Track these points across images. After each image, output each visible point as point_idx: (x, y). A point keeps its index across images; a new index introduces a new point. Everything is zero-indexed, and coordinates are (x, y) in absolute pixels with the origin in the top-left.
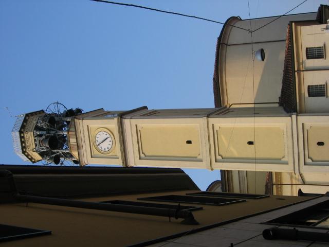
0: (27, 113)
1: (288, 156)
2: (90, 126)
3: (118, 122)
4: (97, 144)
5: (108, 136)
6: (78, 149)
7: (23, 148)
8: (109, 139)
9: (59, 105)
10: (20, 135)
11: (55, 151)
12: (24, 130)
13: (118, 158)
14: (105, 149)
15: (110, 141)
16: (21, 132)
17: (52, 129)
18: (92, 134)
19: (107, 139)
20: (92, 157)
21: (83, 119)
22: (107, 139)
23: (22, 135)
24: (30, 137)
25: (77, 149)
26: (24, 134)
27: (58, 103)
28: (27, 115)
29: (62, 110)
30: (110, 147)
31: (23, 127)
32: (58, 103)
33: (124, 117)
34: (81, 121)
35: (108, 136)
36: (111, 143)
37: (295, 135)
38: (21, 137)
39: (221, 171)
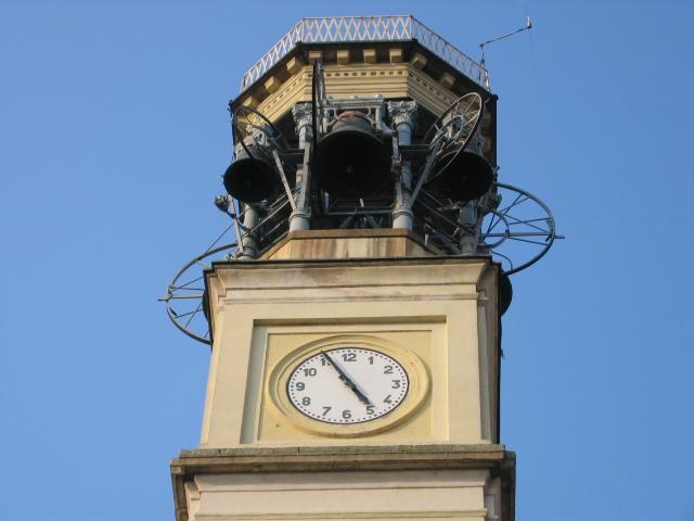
0: (501, 107)
1: (360, 117)
2: (441, 331)
3: (468, 450)
4: (337, 357)
5: (381, 408)
6: (308, 265)
7: (328, 51)
8: (359, 411)
9: (542, 239)
10: (395, 44)
11: (302, 175)
12: (417, 65)
13: (241, 442)
14: (302, 387)
15: (346, 414)
16: (410, 48)
17: (423, 178)
18: (399, 342)
19: (363, 399)
20: (258, 324)
21: (480, 303)
22: (363, 399)
23: (395, 53)
24: (385, 84)
25: (307, 257)
26: (397, 60)
27: (552, 236)
28: (491, 101)
29: (509, 254)
30: (315, 409)
31: (435, 67)
32: (552, 236)
33: (496, 490)
34: (472, 289)
35: (381, 408)
36: (335, 415)
37: (286, 293)
38: (382, 50)
39: (445, 317)
